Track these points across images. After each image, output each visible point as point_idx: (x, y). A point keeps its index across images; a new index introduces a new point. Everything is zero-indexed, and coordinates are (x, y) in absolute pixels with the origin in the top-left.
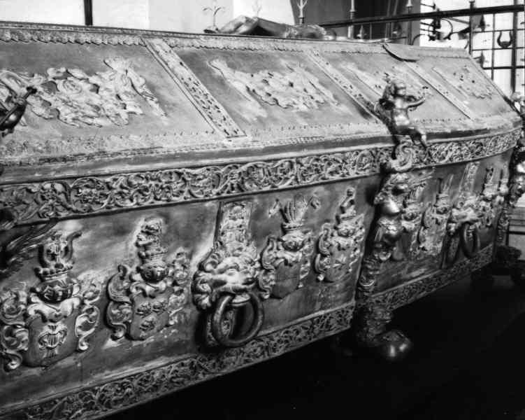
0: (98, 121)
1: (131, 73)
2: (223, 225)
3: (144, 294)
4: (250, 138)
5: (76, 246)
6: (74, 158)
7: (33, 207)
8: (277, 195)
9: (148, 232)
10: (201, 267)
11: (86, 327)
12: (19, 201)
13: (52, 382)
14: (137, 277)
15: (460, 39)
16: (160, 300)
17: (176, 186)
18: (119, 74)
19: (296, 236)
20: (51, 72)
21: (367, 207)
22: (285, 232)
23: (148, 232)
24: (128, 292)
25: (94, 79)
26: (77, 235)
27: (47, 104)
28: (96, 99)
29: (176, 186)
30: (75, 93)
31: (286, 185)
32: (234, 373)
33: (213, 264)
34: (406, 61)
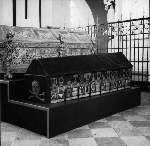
0: (22, 37)
1: (27, 32)
2: (36, 51)
3: (27, 58)
4: (39, 40)
5: (19, 50)
6: (19, 41)
7: (15, 45)
8: (43, 48)
9: (27, 50)
10: (34, 56)
11: (21, 61)
12: (14, 45)
13: (17, 67)
14: (26, 56)
15: (47, 26)
16: (28, 59)
17: (30, 45)
18: (26, 33)
19: (46, 54)
20: (18, 32)
21: (58, 53)
22: (45, 54)
23: (27, 50)
24: (25, 57)
25: (22, 33)
26: (19, 49)
27: (17, 35)
28: (22, 35)
29: (30, 45)
30: (20, 34)
31: (44, 47)
32: (73, 129)
33: (35, 56)
34: (104, 39)
